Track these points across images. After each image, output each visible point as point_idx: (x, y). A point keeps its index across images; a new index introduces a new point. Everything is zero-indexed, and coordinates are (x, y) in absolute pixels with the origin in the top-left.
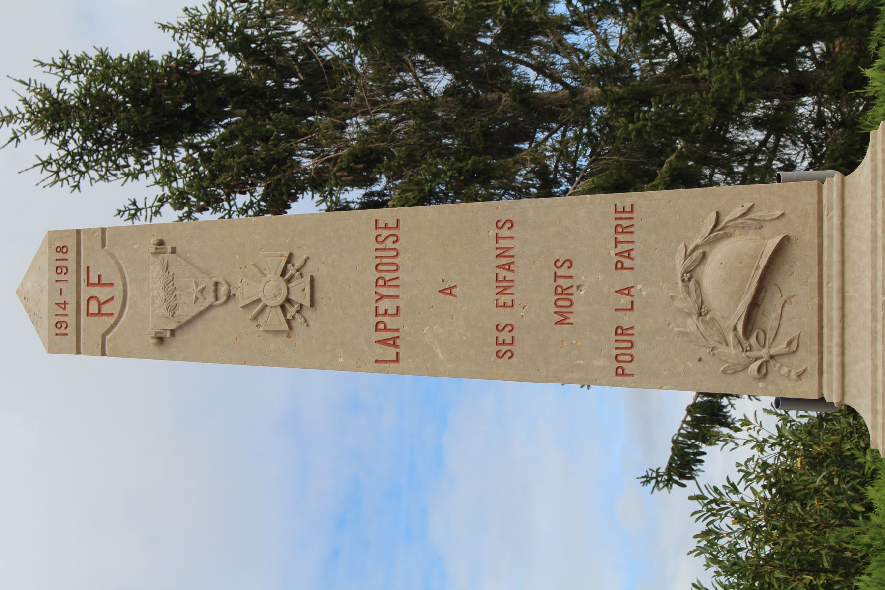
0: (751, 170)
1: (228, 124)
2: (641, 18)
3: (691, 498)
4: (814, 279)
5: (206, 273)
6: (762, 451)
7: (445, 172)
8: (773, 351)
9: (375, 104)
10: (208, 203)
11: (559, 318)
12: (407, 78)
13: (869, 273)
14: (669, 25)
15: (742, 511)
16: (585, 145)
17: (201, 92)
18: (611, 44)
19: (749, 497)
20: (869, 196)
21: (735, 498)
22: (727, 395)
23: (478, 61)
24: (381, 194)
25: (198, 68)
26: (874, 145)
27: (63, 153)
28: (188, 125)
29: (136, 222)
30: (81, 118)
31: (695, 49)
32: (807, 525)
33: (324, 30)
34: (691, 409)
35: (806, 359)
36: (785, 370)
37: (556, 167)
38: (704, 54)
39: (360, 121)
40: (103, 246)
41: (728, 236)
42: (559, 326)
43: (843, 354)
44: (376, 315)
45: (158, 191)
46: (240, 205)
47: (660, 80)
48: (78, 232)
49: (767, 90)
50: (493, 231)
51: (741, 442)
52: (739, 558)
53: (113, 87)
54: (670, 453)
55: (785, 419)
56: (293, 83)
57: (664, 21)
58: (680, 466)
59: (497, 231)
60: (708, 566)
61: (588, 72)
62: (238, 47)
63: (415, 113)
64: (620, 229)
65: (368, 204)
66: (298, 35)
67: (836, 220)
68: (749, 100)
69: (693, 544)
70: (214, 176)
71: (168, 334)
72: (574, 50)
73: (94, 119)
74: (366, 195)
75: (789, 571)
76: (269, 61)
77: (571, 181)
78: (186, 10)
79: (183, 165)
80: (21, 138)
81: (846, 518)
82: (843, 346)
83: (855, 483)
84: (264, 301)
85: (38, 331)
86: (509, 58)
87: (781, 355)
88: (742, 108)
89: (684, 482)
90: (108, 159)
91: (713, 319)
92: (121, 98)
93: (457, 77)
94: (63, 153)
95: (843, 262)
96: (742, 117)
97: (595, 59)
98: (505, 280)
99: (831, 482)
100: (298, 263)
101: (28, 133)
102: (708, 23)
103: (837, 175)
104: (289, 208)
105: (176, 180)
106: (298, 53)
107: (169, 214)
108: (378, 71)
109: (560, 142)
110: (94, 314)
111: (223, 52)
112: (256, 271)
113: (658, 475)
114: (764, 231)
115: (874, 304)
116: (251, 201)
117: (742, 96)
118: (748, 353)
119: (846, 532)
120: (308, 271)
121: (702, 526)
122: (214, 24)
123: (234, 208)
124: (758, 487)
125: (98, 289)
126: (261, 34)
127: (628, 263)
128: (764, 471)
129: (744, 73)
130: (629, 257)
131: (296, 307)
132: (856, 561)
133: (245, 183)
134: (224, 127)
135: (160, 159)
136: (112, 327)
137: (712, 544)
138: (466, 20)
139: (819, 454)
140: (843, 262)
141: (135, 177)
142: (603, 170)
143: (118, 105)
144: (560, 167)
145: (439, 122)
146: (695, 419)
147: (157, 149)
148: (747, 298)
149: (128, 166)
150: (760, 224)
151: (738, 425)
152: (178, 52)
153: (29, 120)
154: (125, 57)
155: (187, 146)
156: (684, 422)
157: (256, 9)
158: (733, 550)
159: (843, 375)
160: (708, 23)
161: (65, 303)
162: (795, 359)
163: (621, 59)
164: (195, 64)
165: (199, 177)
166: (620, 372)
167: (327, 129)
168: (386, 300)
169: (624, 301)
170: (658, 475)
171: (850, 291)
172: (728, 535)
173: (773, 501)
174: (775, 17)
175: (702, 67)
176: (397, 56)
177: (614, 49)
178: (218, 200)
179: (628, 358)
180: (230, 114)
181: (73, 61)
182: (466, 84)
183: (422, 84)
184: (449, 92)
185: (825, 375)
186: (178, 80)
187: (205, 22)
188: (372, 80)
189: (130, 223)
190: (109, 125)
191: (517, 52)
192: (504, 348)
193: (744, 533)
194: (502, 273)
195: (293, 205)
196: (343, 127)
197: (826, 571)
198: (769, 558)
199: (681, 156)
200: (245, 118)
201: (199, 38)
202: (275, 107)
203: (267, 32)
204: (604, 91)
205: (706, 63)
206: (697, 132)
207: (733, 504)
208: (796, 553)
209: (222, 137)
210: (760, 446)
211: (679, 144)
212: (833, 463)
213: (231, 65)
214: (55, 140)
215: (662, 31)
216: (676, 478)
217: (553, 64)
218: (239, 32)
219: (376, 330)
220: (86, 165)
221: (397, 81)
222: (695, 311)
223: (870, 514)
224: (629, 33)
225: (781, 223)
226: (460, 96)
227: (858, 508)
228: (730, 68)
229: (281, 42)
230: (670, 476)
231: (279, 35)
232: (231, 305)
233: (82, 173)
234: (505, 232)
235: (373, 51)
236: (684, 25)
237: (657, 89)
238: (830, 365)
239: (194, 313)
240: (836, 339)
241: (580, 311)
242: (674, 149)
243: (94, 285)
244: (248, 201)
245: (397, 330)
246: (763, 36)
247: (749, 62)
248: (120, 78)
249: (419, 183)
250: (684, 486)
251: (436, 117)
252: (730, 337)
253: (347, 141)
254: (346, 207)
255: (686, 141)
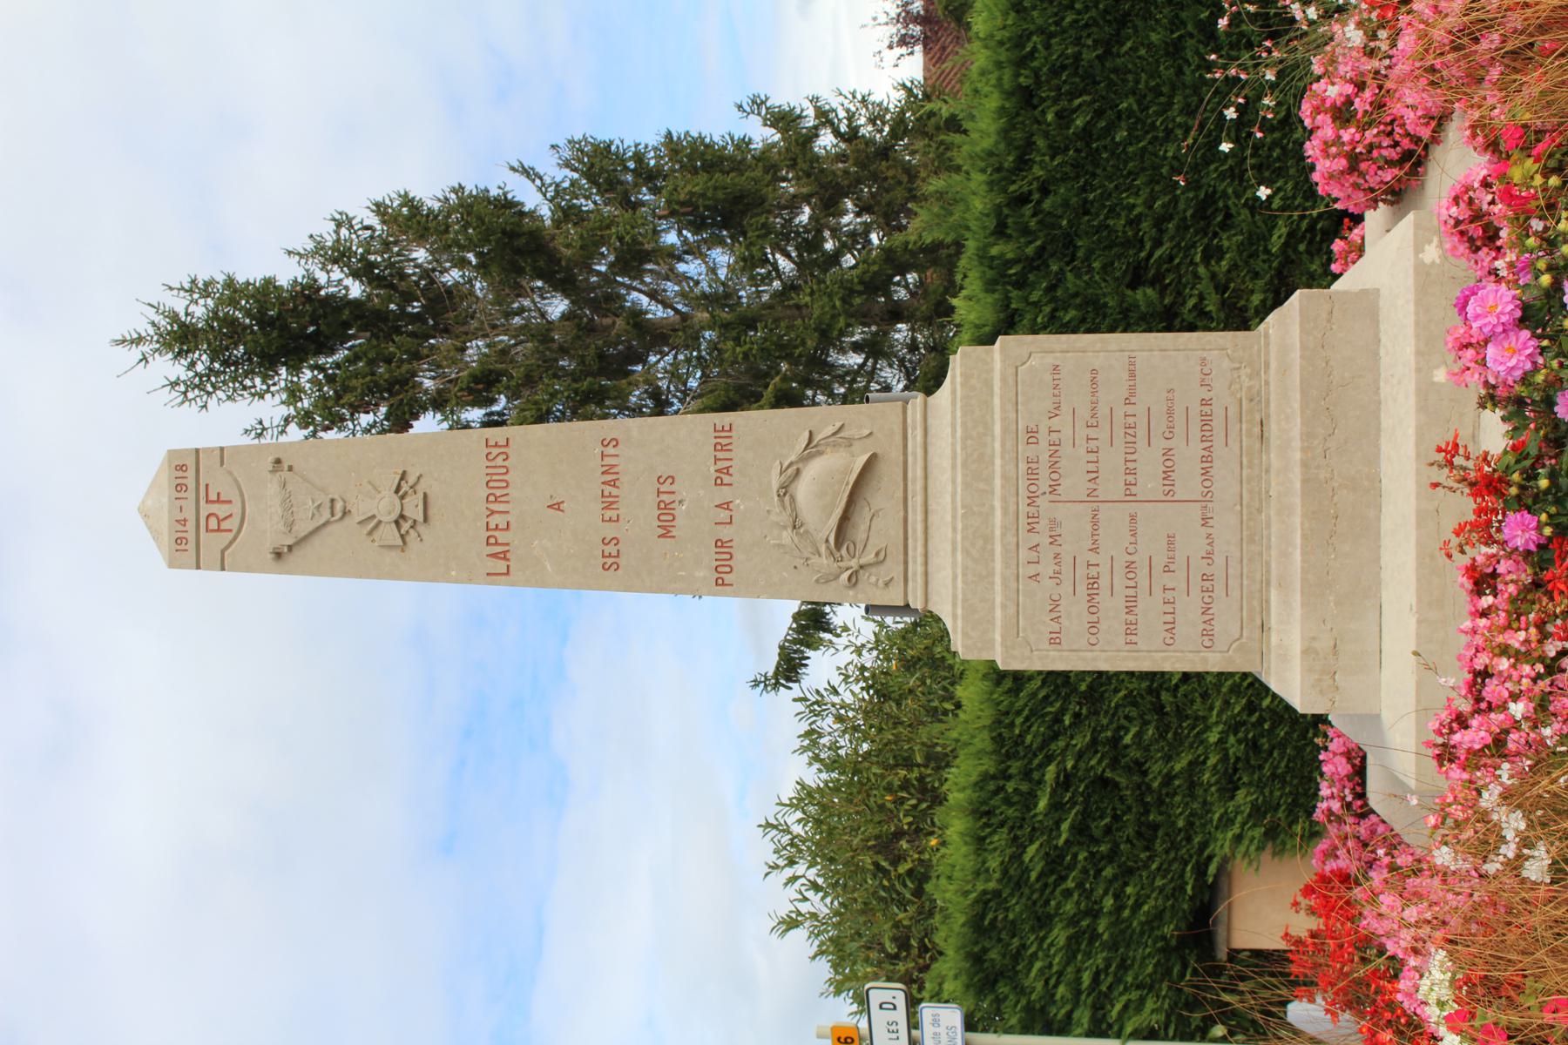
0: (850, 390)
1: (353, 346)
2: (747, 248)
3: (795, 700)
4: (900, 494)
5: (323, 490)
6: (860, 655)
7: (562, 392)
8: (863, 561)
9: (494, 327)
10: (333, 422)
11: (662, 531)
12: (526, 303)
13: (949, 488)
14: (773, 255)
15: (842, 712)
16: (695, 367)
17: (325, 316)
18: (719, 272)
19: (849, 699)
20: (949, 417)
21: (836, 699)
22: (830, 604)
23: (593, 288)
24: (500, 414)
25: (322, 293)
26: (953, 369)
27: (191, 374)
28: (313, 347)
29: (263, 441)
30: (208, 341)
31: (799, 277)
32: (902, 723)
33: (445, 257)
34: (797, 617)
35: (893, 568)
36: (873, 579)
37: (668, 387)
38: (806, 282)
39: (480, 343)
40: (222, 463)
41: (820, 453)
42: (662, 540)
43: (926, 563)
44: (488, 529)
45: (285, 411)
46: (364, 424)
47: (769, 306)
48: (197, 451)
49: (865, 316)
50: (599, 449)
51: (840, 648)
52: (838, 755)
53: (240, 310)
54: (777, 658)
55: (882, 625)
56: (415, 307)
57: (769, 251)
58: (786, 670)
59: (602, 448)
60: (810, 764)
61: (697, 298)
62: (361, 272)
63: (533, 336)
64: (719, 447)
65: (488, 423)
66: (420, 261)
67: (919, 439)
68: (848, 325)
69: (797, 743)
70: (338, 397)
71: (286, 550)
72: (685, 277)
73: (221, 340)
74: (487, 414)
75: (887, 767)
76: (392, 286)
77: (681, 401)
78: (311, 236)
79: (308, 385)
80: (150, 359)
81: (936, 714)
82: (926, 555)
83: (945, 683)
84: (379, 518)
85: (159, 547)
86: (623, 284)
87: (870, 565)
88: (842, 333)
89: (790, 685)
90: (234, 380)
91: (807, 532)
92: (248, 321)
93: (572, 302)
94: (191, 374)
95: (926, 478)
96: (842, 342)
97: (704, 285)
98: (610, 496)
99: (924, 683)
100: (411, 479)
101: (157, 355)
102: (810, 253)
103: (920, 396)
104: (411, 426)
105: (301, 400)
106: (421, 278)
107: (295, 433)
108: (497, 294)
109: (671, 365)
110: (213, 531)
111: (347, 276)
112: (370, 487)
113: (766, 679)
114: (853, 448)
115: (954, 517)
116: (375, 422)
117: (842, 322)
118: (840, 564)
119: (938, 727)
120: (421, 488)
121: (805, 727)
122: (339, 250)
123: (358, 428)
124: (856, 688)
125: (216, 505)
126: (384, 260)
127: (726, 479)
128: (862, 674)
129: (843, 300)
130: (728, 473)
131: (410, 523)
132: (947, 755)
133: (369, 403)
134: (349, 349)
135: (286, 380)
136: (231, 543)
137: (814, 743)
138: (582, 247)
139: (912, 657)
140: (926, 478)
141: (261, 396)
142: (712, 391)
143: (245, 327)
144: (672, 388)
145: (555, 346)
146: (800, 626)
147: (283, 371)
148: (838, 512)
149: (254, 387)
150: (849, 442)
151: (839, 631)
152: (304, 277)
153: (158, 342)
154: (252, 281)
155: (312, 368)
156: (790, 628)
157: (379, 236)
158: (834, 747)
159: (926, 583)
160: (810, 253)
161: (185, 520)
162: (882, 569)
163: (728, 286)
164: (320, 288)
165: (324, 398)
166: (720, 583)
167: (449, 351)
168: (497, 515)
169: (723, 515)
170: (766, 679)
171: (932, 506)
172: (830, 734)
173: (871, 701)
174: (871, 250)
175: (805, 295)
176: (515, 282)
177: (723, 278)
178: (343, 419)
179: (728, 569)
180: (354, 337)
181: (200, 285)
182: (581, 309)
183: (539, 309)
184: (565, 317)
185: (910, 584)
186: (304, 304)
187: (330, 248)
188: (492, 304)
189: (256, 441)
190: (236, 347)
191: (630, 278)
192: (611, 561)
193: (844, 732)
194: (608, 489)
195: (415, 423)
196: (463, 350)
197: (918, 766)
198: (868, 753)
199: (785, 379)
200: (369, 340)
201: (323, 264)
202: (397, 330)
203: (390, 258)
204: (713, 317)
205: (808, 291)
206: (800, 355)
207: (834, 705)
208: (892, 750)
209: (347, 360)
210: (858, 651)
211: (784, 366)
212: (926, 664)
213: (356, 290)
214: (183, 361)
215: (767, 260)
216: (782, 681)
217: (665, 291)
218: (363, 258)
219: (488, 544)
220: (213, 385)
221: (516, 305)
222: (790, 524)
223: (958, 712)
224: (736, 262)
225: (868, 441)
226: (576, 320)
227: (948, 706)
228: (830, 296)
229: (404, 268)
230: (777, 680)
231: (401, 261)
232: (347, 520)
233: (209, 394)
234: (610, 450)
235: (492, 277)
236: (788, 256)
237: (762, 315)
238: (915, 574)
239: (311, 528)
240: (920, 550)
241: (681, 525)
242: (778, 373)
243: (213, 502)
244: (371, 422)
245: (507, 544)
246: (861, 266)
247: (849, 292)
248: (247, 302)
249: (536, 403)
250: (790, 688)
251: (553, 340)
252: (823, 549)
253: (467, 362)
254: (467, 426)
255: (790, 364)
